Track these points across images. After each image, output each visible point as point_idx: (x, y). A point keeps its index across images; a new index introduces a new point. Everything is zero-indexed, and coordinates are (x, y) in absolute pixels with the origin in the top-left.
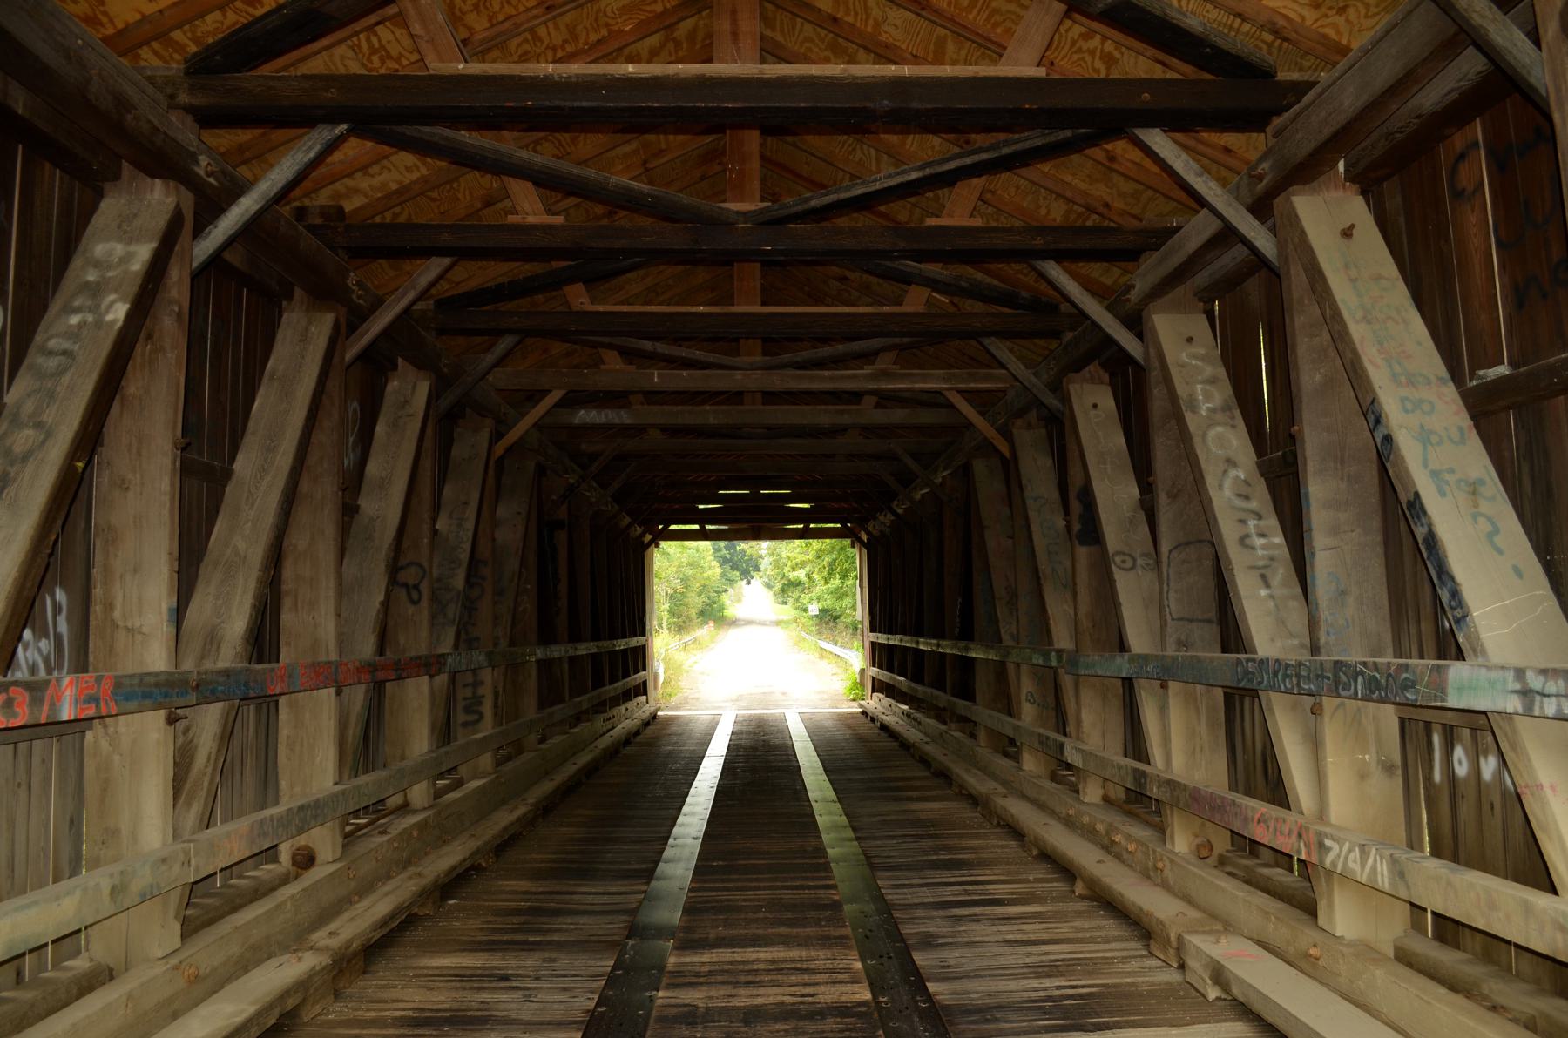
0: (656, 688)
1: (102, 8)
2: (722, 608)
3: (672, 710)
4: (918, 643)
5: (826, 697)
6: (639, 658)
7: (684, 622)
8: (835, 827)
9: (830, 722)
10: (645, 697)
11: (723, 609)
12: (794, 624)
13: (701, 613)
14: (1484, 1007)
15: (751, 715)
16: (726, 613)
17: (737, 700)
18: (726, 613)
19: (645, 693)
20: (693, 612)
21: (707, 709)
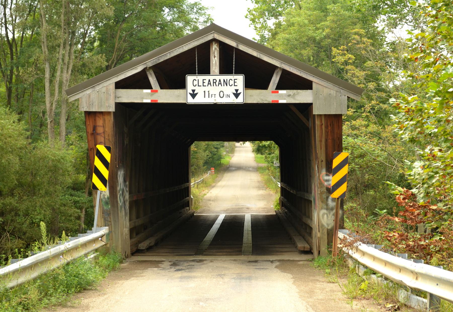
0: (192, 205)
1: (15, 287)
2: (220, 158)
3: (199, 213)
4: (291, 190)
5: (265, 209)
6: (187, 191)
7: (195, 169)
8: (86, 250)
9: (261, 217)
10: (188, 208)
11: (221, 158)
12: (267, 171)
13: (206, 163)
14: (380, 273)
15: (228, 215)
16: (223, 161)
17: (226, 210)
18: (223, 161)
19: (188, 206)
20: (201, 163)
21: (214, 213)
